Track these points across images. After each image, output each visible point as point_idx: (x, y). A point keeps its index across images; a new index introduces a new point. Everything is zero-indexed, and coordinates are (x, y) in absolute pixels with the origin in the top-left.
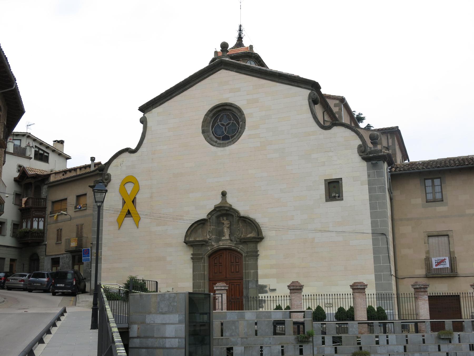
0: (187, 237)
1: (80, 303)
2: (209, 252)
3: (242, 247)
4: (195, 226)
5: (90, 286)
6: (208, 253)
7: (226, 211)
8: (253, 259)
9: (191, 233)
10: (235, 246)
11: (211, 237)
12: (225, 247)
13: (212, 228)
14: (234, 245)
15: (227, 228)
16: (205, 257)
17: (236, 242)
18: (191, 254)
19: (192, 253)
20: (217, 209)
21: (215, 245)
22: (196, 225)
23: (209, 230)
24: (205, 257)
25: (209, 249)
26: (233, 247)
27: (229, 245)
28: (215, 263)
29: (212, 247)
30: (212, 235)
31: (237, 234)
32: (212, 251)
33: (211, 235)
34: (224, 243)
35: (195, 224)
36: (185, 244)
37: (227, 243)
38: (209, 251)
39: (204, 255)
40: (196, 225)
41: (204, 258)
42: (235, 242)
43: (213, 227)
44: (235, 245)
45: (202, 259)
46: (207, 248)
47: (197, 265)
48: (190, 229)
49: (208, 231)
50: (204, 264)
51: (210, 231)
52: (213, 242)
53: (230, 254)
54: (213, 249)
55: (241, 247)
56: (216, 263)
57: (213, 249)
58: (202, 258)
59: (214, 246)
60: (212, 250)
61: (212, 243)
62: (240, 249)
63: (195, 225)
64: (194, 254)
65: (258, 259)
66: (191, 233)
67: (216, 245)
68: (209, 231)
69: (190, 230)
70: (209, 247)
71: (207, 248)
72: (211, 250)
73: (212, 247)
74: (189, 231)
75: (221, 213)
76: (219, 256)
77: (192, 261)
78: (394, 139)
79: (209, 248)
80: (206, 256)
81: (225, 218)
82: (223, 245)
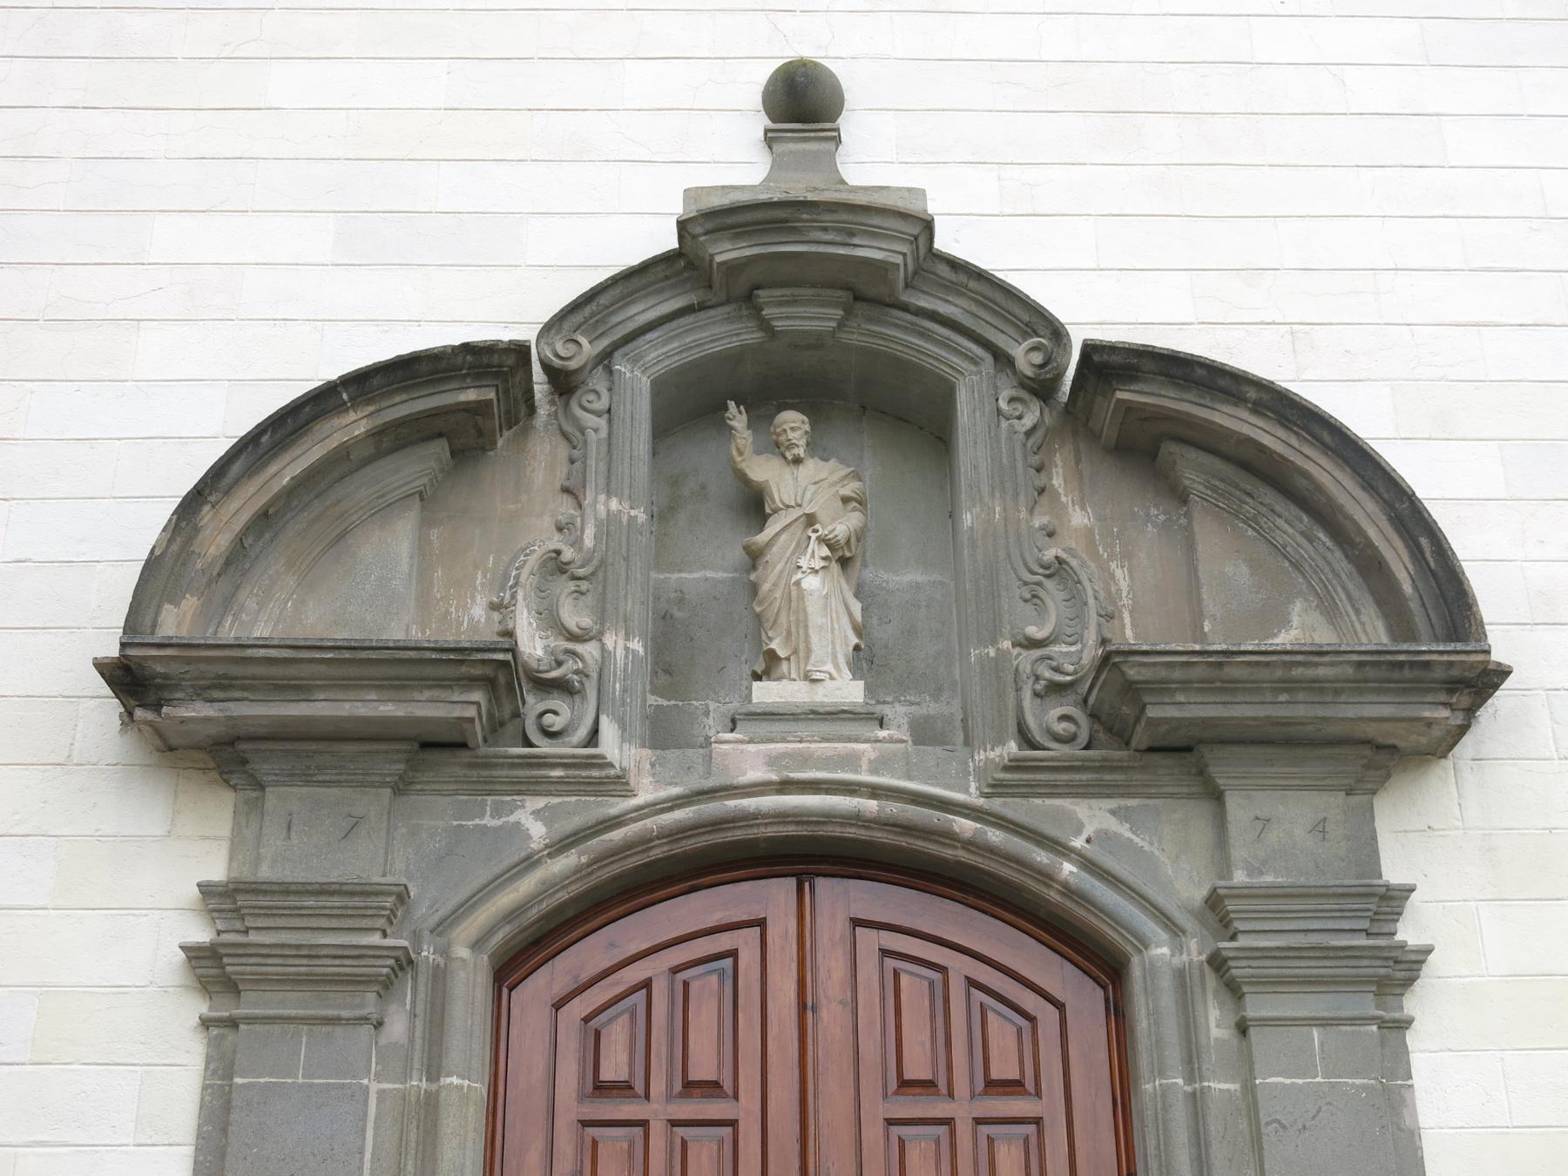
0: (175, 600)
1: (586, 641)
2: (527, 885)
3: (1113, 825)
4: (333, 443)
5: (644, 946)
6: (506, 899)
7: (848, 311)
8: (1323, 1022)
9: (238, 557)
10: (996, 804)
11: (589, 650)
12: (828, 817)
13: (608, 527)
14: (971, 795)
15: (825, 552)
16: (462, 952)
17: (1027, 741)
18: (206, 890)
19: (217, 871)
20: (726, 252)
21: (647, 780)
22: (353, 425)
23: (556, 542)
24: (462, 952)
25: (538, 831)
26: (965, 826)
27: (875, 791)
28: (601, 1089)
29: (583, 810)
30: (602, 616)
31: (1034, 631)
32: (578, 872)
33: (574, 617)
34: (805, 760)
35: (341, 408)
36: (105, 707)
37: (851, 761)
38: (530, 862)
39: (443, 926)
40: (353, 425)
41: (440, 976)
42: (1012, 747)
43: (614, 504)
44: (997, 789)
45: (386, 986)
46: (497, 813)
47: (300, 1080)
48: (250, 472)
49: (533, 561)
50: (418, 1083)
51: (568, 554)
52: (609, 730)
53: (870, 940)
54: (617, 835)
55: (1103, 838)
56: (623, 1089)
57: (617, 835)
58: (404, 963)
59: (619, 784)
60: (597, 843)
61: (593, 737)
62: (1088, 865)
63: (338, 422)
64: (255, 889)
65: (1404, 1024)
66: (238, 557)
67: (659, 782)
68: (556, 566)
69: (251, 487)
70: (540, 802)
71: (488, 821)
72: (560, 846)
73: (583, 810)
74: (234, 504)
75: (749, 336)
76: (675, 970)
77: (198, 1007)
78: (725, 571)
79: (537, 814)
80: (476, 945)
81: (793, 424)
82: (785, 786)
